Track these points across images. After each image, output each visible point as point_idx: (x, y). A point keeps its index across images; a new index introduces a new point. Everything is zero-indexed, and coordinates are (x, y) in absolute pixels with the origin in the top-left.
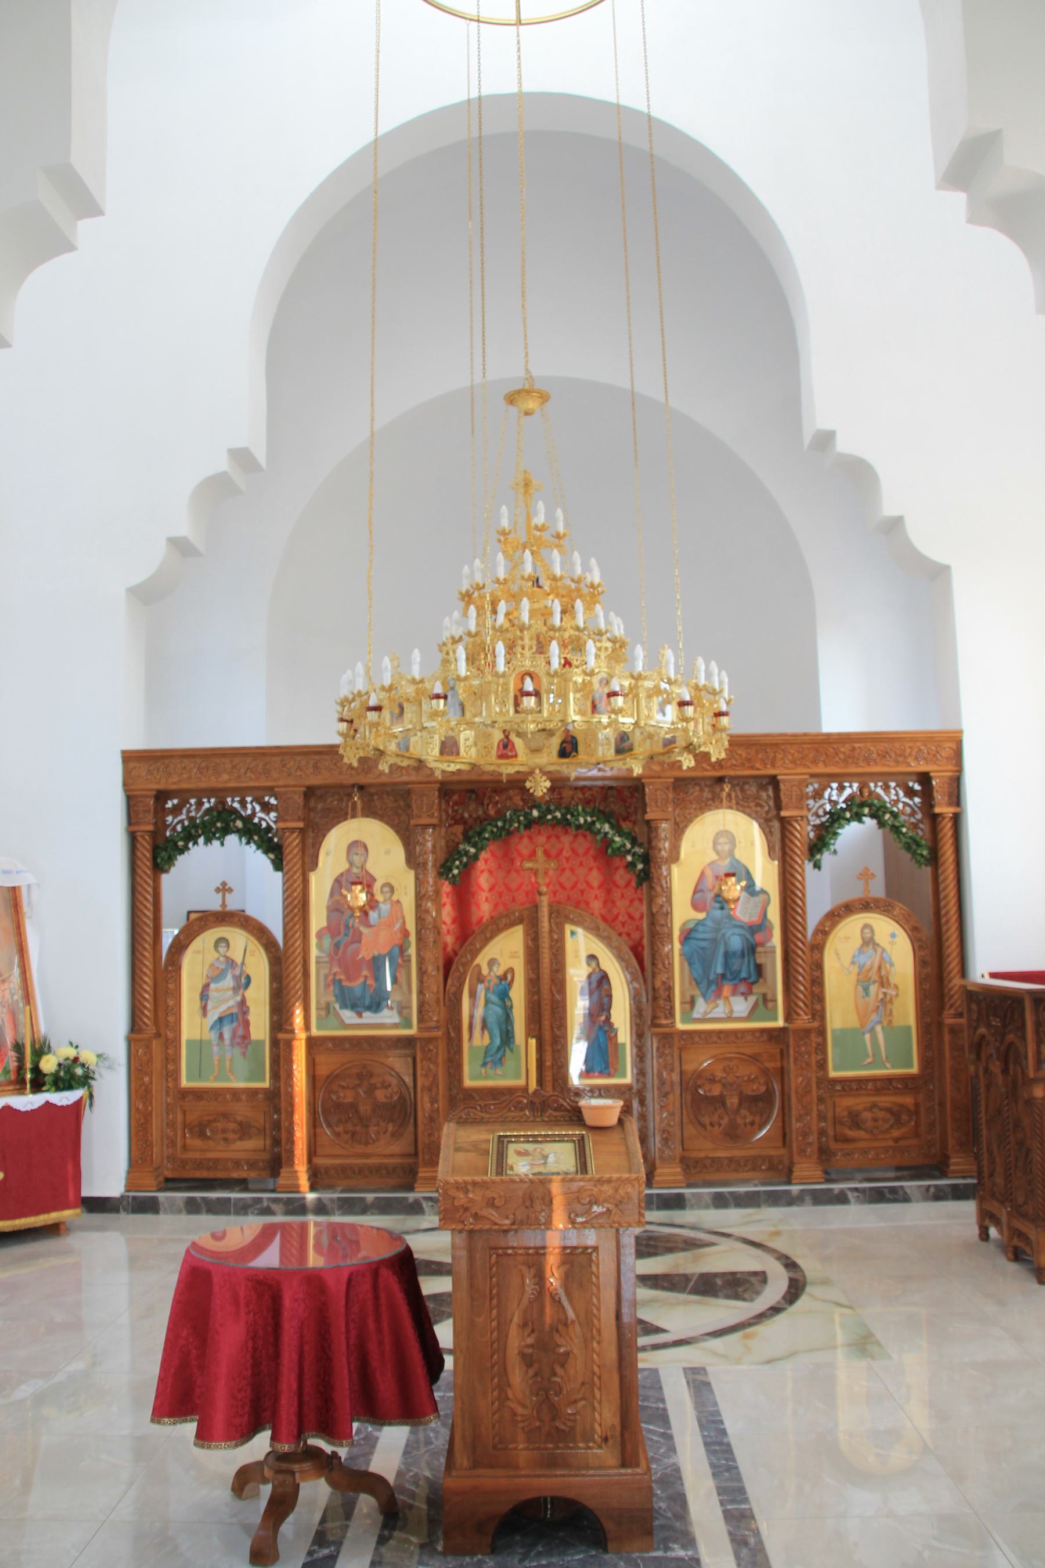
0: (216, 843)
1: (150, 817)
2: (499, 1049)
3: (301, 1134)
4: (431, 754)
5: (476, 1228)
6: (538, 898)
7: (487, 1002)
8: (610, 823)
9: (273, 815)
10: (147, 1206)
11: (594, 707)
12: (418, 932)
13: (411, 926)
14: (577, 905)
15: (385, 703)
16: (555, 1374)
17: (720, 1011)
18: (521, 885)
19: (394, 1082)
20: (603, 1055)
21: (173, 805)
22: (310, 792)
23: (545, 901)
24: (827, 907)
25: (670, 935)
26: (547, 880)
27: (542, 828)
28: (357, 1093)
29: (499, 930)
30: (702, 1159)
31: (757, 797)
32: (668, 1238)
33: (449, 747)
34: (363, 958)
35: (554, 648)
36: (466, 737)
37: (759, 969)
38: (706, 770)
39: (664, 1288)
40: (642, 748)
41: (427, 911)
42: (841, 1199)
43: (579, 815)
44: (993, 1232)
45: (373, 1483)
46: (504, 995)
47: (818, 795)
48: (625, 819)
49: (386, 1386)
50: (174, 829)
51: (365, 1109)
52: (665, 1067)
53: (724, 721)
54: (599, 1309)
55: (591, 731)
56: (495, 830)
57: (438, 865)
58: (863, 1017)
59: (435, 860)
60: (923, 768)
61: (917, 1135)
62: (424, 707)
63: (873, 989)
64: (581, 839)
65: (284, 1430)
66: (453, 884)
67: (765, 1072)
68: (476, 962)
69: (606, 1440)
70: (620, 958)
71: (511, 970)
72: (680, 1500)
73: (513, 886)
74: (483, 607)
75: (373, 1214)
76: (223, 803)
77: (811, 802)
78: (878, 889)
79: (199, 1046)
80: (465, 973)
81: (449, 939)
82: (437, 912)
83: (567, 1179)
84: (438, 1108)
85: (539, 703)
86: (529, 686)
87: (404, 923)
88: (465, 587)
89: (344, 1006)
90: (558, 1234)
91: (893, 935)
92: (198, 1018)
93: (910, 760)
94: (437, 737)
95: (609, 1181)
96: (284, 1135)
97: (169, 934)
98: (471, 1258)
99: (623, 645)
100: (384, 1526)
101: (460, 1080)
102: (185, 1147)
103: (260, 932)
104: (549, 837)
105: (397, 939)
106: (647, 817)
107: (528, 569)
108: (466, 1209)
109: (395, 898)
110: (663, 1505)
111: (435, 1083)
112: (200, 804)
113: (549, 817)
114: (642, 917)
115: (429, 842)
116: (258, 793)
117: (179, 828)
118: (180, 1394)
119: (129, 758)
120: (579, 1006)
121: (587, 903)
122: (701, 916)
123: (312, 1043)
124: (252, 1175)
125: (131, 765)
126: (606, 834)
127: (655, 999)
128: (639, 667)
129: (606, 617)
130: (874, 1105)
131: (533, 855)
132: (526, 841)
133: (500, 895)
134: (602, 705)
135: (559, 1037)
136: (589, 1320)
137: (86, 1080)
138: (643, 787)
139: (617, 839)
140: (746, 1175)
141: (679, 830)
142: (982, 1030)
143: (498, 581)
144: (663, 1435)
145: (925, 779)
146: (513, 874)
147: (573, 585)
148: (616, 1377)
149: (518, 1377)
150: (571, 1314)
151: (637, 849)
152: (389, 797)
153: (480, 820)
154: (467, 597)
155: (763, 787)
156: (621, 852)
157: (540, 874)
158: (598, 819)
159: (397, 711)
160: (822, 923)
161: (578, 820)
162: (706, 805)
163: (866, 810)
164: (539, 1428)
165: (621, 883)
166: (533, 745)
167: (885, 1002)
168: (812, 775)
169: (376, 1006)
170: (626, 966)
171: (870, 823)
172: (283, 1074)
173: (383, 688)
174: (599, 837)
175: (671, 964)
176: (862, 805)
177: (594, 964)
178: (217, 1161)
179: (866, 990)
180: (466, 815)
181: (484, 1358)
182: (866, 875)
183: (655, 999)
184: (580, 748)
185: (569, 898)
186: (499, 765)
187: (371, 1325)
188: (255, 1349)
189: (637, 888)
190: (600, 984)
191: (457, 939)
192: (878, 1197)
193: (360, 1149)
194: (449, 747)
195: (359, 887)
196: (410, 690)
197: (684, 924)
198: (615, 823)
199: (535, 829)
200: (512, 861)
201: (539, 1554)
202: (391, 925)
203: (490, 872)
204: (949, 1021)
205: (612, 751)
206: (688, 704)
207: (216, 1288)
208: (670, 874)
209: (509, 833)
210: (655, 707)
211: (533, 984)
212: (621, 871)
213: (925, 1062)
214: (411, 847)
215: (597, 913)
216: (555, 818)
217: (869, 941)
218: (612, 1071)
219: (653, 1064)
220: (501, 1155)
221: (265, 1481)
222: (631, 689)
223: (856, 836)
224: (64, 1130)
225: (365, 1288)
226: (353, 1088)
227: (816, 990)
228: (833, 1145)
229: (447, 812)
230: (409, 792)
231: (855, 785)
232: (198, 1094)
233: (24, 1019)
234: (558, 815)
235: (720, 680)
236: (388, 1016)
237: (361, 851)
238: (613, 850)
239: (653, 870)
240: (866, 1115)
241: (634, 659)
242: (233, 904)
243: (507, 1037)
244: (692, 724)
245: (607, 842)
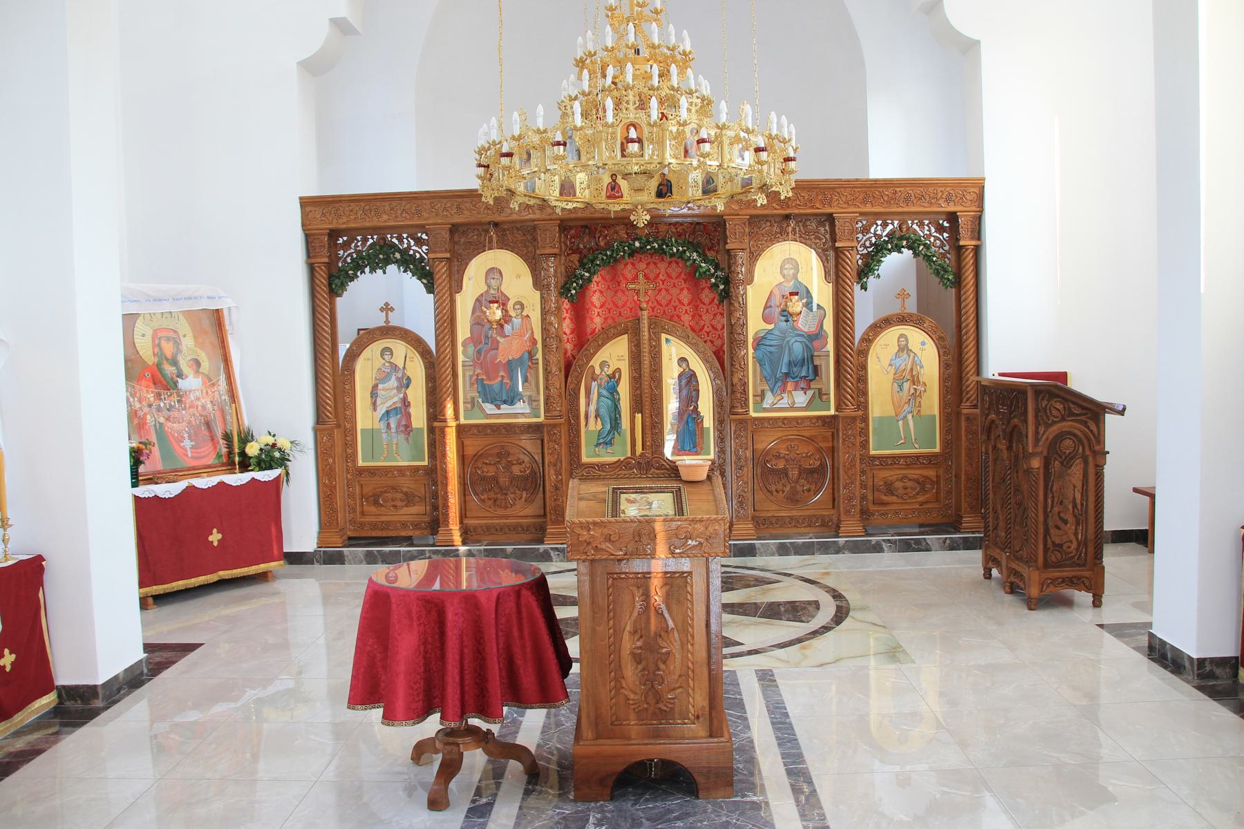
0: (379, 271)
1: (325, 251)
2: (609, 432)
3: (454, 501)
4: (553, 195)
5: (597, 557)
7: (600, 395)
9: (424, 248)
10: (335, 559)
11: (686, 151)
12: (544, 340)
13: (538, 336)
15: (515, 151)
16: (659, 669)
17: (785, 402)
19: (527, 459)
20: (691, 438)
21: (344, 239)
22: (454, 229)
24: (871, 321)
25: (745, 342)
29: (608, 339)
31: (816, 232)
32: (742, 578)
33: (567, 189)
35: (654, 103)
36: (581, 178)
37: (816, 370)
39: (739, 614)
40: (724, 189)
41: (551, 324)
42: (877, 548)
44: (995, 572)
45: (519, 752)
46: (613, 391)
47: (865, 230)
49: (528, 680)
50: (345, 261)
51: (504, 480)
52: (741, 447)
53: (792, 165)
54: (692, 620)
55: (683, 174)
58: (897, 407)
60: (952, 208)
61: (937, 500)
62: (548, 153)
63: (906, 385)
64: (674, 265)
65: (450, 711)
66: (572, 302)
67: (819, 450)
69: (698, 717)
71: (619, 370)
72: (752, 761)
73: (620, 303)
74: (595, 72)
76: (384, 239)
77: (860, 236)
78: (911, 307)
79: (371, 434)
80: (581, 374)
81: (569, 347)
83: (667, 520)
85: (642, 148)
86: (633, 134)
88: (579, 54)
90: (660, 563)
91: (923, 344)
92: (369, 412)
93: (941, 202)
94: (556, 178)
95: (701, 521)
96: (441, 501)
97: (343, 349)
98: (592, 582)
99: (710, 103)
100: (529, 783)
101: (579, 457)
102: (363, 513)
103: (415, 341)
104: (648, 264)
105: (527, 346)
106: (727, 247)
107: (631, 38)
108: (589, 544)
110: (741, 766)
112: (365, 240)
115: (552, 268)
116: (412, 231)
117: (349, 260)
118: (368, 688)
119: (305, 203)
120: (672, 405)
121: (679, 317)
122: (771, 327)
123: (461, 430)
124: (415, 533)
125: (308, 209)
127: (733, 392)
128: (723, 118)
129: (696, 79)
130: (905, 477)
131: (636, 277)
132: (630, 267)
133: (609, 310)
134: (693, 151)
136: (685, 628)
137: (283, 461)
140: (803, 530)
141: (754, 257)
142: (993, 416)
143: (606, 49)
144: (739, 717)
145: (953, 217)
146: (620, 294)
147: (669, 53)
148: (705, 671)
149: (630, 672)
150: (671, 624)
151: (719, 273)
152: (518, 231)
153: (592, 250)
154: (580, 64)
155: (821, 224)
156: (706, 275)
157: (642, 293)
159: (525, 156)
160: (866, 333)
163: (905, 243)
164: (646, 709)
165: (707, 301)
166: (637, 186)
167: (915, 396)
168: (862, 214)
169: (511, 401)
170: (710, 368)
171: (907, 253)
172: (438, 454)
173: (513, 138)
175: (746, 365)
176: (901, 238)
178: (388, 523)
179: (901, 387)
181: (603, 659)
182: (903, 295)
183: (733, 392)
187: (516, 634)
188: (426, 652)
190: (689, 381)
192: (906, 547)
193: (501, 512)
194: (567, 189)
196: (536, 139)
198: (700, 252)
200: (619, 283)
201: (647, 800)
203: (601, 292)
204: (965, 411)
206: (763, 150)
207: (394, 606)
208: (745, 293)
209: (616, 260)
210: (736, 153)
211: (636, 381)
212: (707, 291)
213: (946, 444)
215: (687, 324)
216: (653, 248)
217: (904, 348)
219: (731, 444)
220: (616, 503)
221: (437, 752)
222: (716, 137)
223: (896, 263)
224: (265, 504)
225: (510, 605)
227: (861, 387)
228: (872, 508)
230: (534, 228)
231: (896, 222)
232: (372, 472)
233: (231, 419)
235: (789, 130)
236: (521, 407)
237: (497, 276)
240: (899, 484)
241: (719, 112)
242: (394, 322)
244: (765, 167)
245: (695, 267)
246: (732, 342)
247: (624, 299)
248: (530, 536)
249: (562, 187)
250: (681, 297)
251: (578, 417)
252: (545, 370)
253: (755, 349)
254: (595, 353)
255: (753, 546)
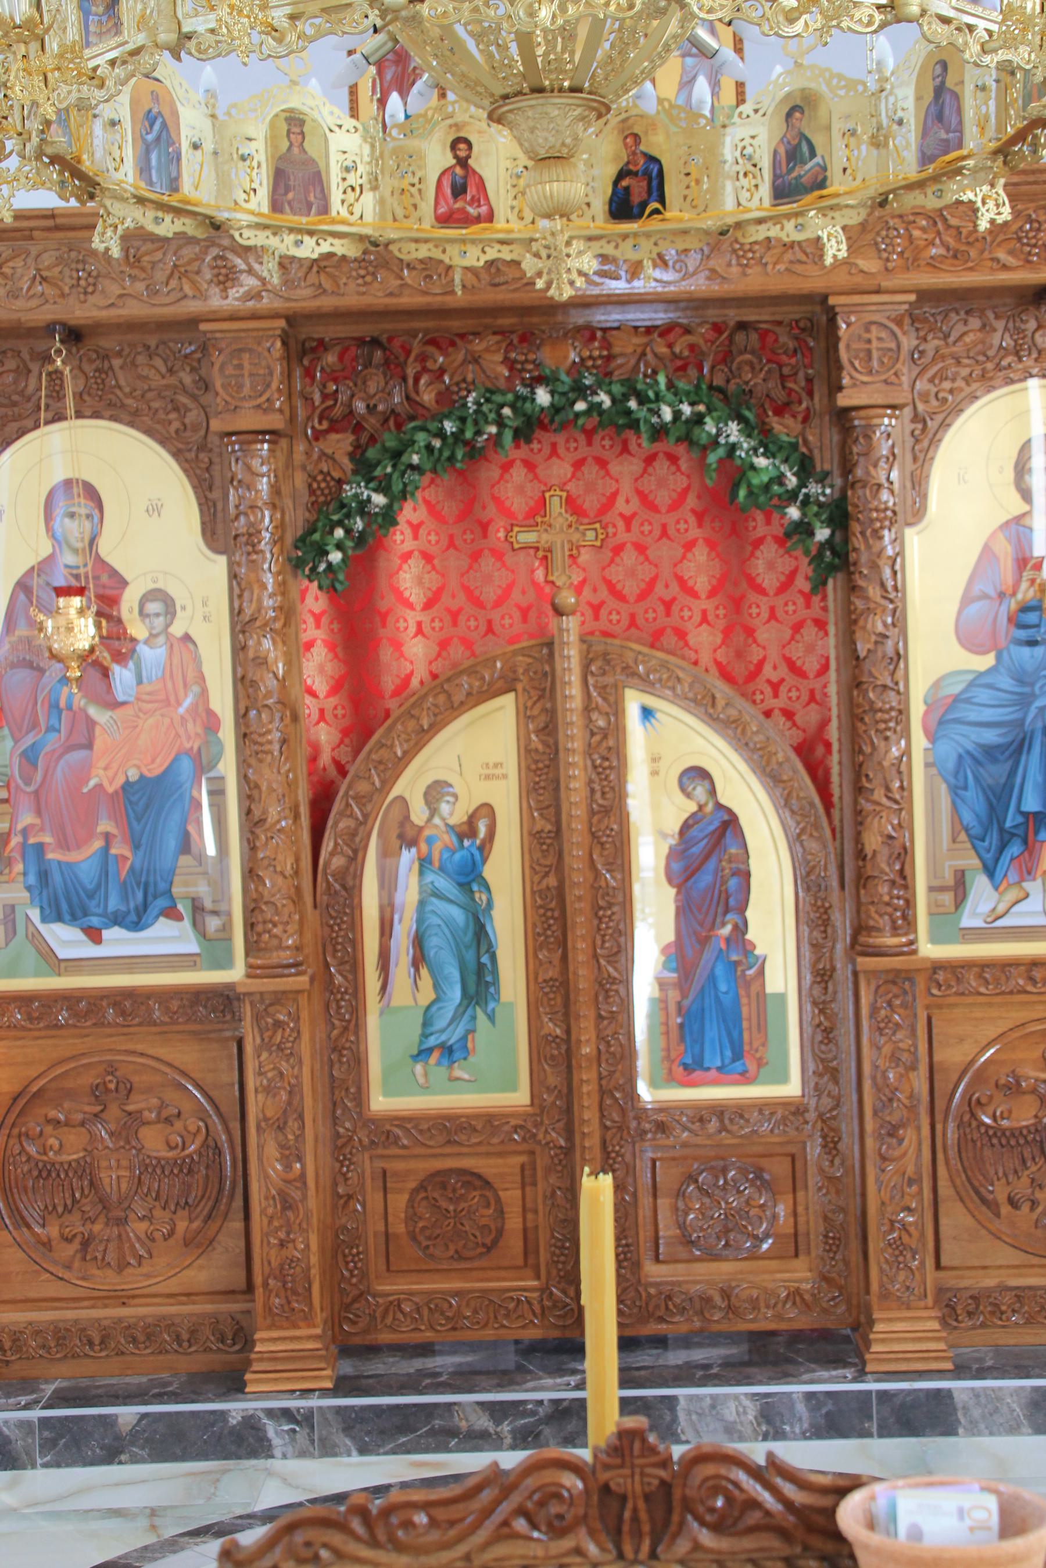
6: (553, 622)
8: (741, 419)
12: (241, 717)
13: (222, 700)
14: (655, 640)
18: (510, 586)
23: (571, 625)
25: (903, 713)
26: (576, 579)
27: (560, 439)
28: (93, 1137)
29: (455, 709)
30: (988, 1292)
34: (99, 786)
38: (1005, 267)
40: (856, 169)
41: (262, 662)
43: (658, 398)
46: (470, 878)
48: (779, 412)
51: (113, 1177)
52: (895, 1059)
56: (437, 443)
57: (289, 539)
59: (281, 527)
64: (662, 466)
68: (395, 792)
70: (771, 776)
71: (487, 810)
73: (489, 594)
75: (135, 1460)
80: (366, 820)
81: (325, 735)
82: (288, 663)
84: (303, 1176)
87: (204, 693)
89: (54, 913)
101: (360, 1096)
104: (578, 464)
106: (843, 400)
109: (177, 629)
111: (293, 1110)
113: (580, 406)
114: (824, 668)
121: (681, 634)
126: (733, 448)
127: (863, 880)
132: (518, 473)
133: (455, 616)
135: (614, 981)
138: (832, 321)
139: (761, 462)
141: (926, 435)
146: (487, 563)
151: (813, 488)
153: (396, 419)
157: (559, 557)
158: (710, 410)
161: (657, 413)
162: (998, 368)
165: (769, 581)
166: (545, 141)
170: (786, 801)
174: (712, 458)
175: (906, 788)
177: (700, 792)
180: (360, 406)
184: (672, 189)
185: (633, 623)
186: (438, 243)
189: (814, 589)
190: (710, 850)
191: (345, 732)
193: (107, 1280)
194: (297, 182)
195: (76, 601)
197: (937, 685)
199: (543, 440)
200: (484, 527)
202: (169, 702)
203: (427, 557)
205: (765, 191)
209: (475, 454)
211: (545, 845)
212: (769, 551)
214: (216, 495)
215: (706, 658)
216: (594, 408)
218: (752, 1067)
226: (82, 1124)
229: (308, 399)
234: (604, 399)
237: (83, 507)
238: (751, 493)
239: (857, 542)
243: (480, 985)
245: (735, 472)
246: (856, 715)
247: (501, 578)
248: (198, 1361)
249: (280, 177)
250: (688, 570)
251: (354, 965)
252: (247, 813)
253: (931, 736)
254: (409, 756)
255: (942, 1397)
